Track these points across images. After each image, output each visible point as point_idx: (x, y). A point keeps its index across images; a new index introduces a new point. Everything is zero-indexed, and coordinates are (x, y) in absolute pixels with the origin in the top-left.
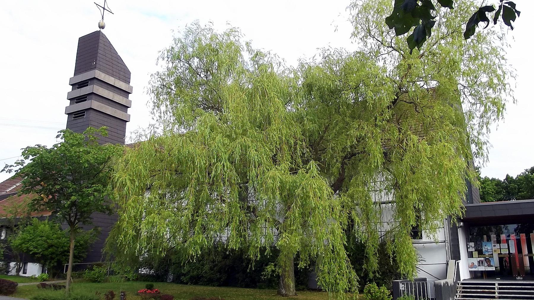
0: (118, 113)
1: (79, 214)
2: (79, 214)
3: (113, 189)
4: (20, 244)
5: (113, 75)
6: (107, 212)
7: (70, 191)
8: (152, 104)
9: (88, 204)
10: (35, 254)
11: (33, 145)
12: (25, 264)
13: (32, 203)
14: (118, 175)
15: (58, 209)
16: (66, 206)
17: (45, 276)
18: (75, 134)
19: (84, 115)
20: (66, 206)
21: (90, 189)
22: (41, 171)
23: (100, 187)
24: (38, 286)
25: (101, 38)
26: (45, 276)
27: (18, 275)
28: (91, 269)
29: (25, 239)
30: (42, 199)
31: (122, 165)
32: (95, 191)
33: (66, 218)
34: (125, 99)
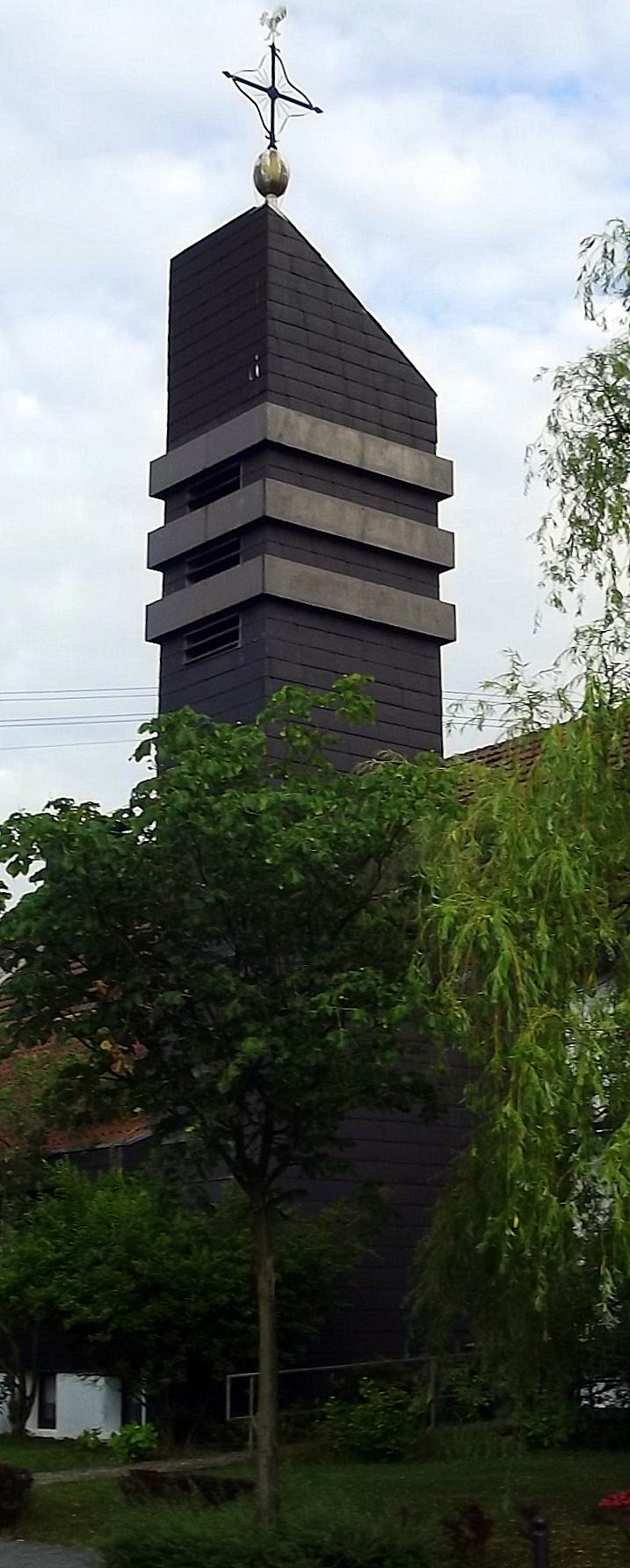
0: (393, 605)
1: (283, 1126)
2: (283, 1126)
3: (437, 980)
4: (16, 1288)
5: (349, 419)
6: (417, 1107)
7: (229, 1014)
8: (561, 532)
9: (321, 1071)
10: (85, 1328)
11: (35, 805)
12: (45, 1383)
13: (59, 1088)
14: (449, 908)
15: (182, 1110)
16: (222, 1087)
17: (140, 1437)
18: (221, 729)
19: (234, 635)
20: (222, 1087)
21: (326, 996)
22: (88, 924)
23: (369, 978)
24: (124, 1485)
25: (273, 241)
26: (142, 1431)
27: (20, 1434)
28: (351, 1395)
29: (32, 1260)
30: (107, 1061)
31: (462, 861)
32: (354, 999)
33: (223, 1151)
34: (420, 529)
